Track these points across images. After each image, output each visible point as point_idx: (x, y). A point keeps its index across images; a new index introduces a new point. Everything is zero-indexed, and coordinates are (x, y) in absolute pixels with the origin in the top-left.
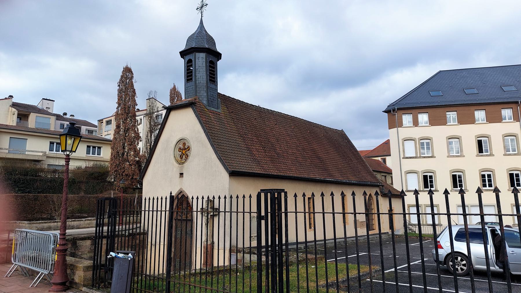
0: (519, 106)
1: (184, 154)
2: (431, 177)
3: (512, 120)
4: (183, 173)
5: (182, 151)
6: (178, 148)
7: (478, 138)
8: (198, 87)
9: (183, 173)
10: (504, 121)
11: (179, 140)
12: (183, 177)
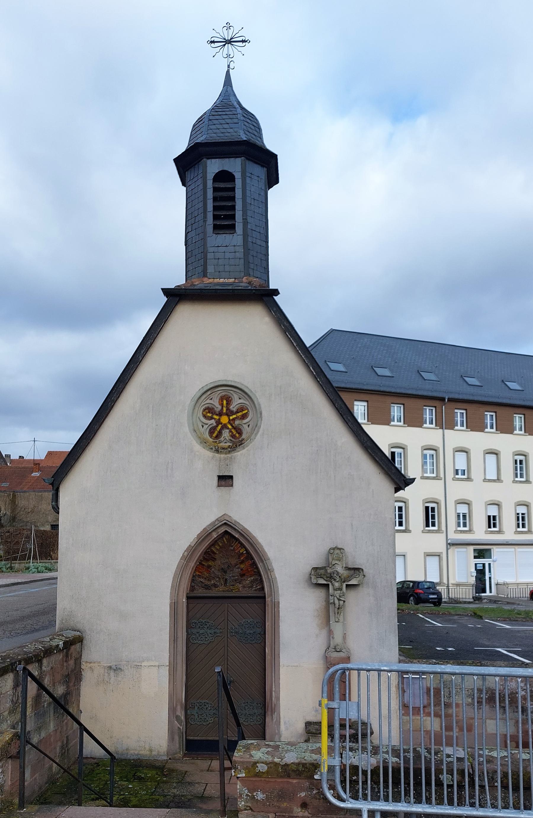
0: (445, 404)
1: (225, 426)
2: (433, 509)
3: (402, 423)
4: (231, 477)
5: (217, 417)
6: (204, 407)
7: (392, 448)
8: (251, 253)
9: (231, 477)
10: (392, 423)
11: (233, 384)
12: (232, 486)
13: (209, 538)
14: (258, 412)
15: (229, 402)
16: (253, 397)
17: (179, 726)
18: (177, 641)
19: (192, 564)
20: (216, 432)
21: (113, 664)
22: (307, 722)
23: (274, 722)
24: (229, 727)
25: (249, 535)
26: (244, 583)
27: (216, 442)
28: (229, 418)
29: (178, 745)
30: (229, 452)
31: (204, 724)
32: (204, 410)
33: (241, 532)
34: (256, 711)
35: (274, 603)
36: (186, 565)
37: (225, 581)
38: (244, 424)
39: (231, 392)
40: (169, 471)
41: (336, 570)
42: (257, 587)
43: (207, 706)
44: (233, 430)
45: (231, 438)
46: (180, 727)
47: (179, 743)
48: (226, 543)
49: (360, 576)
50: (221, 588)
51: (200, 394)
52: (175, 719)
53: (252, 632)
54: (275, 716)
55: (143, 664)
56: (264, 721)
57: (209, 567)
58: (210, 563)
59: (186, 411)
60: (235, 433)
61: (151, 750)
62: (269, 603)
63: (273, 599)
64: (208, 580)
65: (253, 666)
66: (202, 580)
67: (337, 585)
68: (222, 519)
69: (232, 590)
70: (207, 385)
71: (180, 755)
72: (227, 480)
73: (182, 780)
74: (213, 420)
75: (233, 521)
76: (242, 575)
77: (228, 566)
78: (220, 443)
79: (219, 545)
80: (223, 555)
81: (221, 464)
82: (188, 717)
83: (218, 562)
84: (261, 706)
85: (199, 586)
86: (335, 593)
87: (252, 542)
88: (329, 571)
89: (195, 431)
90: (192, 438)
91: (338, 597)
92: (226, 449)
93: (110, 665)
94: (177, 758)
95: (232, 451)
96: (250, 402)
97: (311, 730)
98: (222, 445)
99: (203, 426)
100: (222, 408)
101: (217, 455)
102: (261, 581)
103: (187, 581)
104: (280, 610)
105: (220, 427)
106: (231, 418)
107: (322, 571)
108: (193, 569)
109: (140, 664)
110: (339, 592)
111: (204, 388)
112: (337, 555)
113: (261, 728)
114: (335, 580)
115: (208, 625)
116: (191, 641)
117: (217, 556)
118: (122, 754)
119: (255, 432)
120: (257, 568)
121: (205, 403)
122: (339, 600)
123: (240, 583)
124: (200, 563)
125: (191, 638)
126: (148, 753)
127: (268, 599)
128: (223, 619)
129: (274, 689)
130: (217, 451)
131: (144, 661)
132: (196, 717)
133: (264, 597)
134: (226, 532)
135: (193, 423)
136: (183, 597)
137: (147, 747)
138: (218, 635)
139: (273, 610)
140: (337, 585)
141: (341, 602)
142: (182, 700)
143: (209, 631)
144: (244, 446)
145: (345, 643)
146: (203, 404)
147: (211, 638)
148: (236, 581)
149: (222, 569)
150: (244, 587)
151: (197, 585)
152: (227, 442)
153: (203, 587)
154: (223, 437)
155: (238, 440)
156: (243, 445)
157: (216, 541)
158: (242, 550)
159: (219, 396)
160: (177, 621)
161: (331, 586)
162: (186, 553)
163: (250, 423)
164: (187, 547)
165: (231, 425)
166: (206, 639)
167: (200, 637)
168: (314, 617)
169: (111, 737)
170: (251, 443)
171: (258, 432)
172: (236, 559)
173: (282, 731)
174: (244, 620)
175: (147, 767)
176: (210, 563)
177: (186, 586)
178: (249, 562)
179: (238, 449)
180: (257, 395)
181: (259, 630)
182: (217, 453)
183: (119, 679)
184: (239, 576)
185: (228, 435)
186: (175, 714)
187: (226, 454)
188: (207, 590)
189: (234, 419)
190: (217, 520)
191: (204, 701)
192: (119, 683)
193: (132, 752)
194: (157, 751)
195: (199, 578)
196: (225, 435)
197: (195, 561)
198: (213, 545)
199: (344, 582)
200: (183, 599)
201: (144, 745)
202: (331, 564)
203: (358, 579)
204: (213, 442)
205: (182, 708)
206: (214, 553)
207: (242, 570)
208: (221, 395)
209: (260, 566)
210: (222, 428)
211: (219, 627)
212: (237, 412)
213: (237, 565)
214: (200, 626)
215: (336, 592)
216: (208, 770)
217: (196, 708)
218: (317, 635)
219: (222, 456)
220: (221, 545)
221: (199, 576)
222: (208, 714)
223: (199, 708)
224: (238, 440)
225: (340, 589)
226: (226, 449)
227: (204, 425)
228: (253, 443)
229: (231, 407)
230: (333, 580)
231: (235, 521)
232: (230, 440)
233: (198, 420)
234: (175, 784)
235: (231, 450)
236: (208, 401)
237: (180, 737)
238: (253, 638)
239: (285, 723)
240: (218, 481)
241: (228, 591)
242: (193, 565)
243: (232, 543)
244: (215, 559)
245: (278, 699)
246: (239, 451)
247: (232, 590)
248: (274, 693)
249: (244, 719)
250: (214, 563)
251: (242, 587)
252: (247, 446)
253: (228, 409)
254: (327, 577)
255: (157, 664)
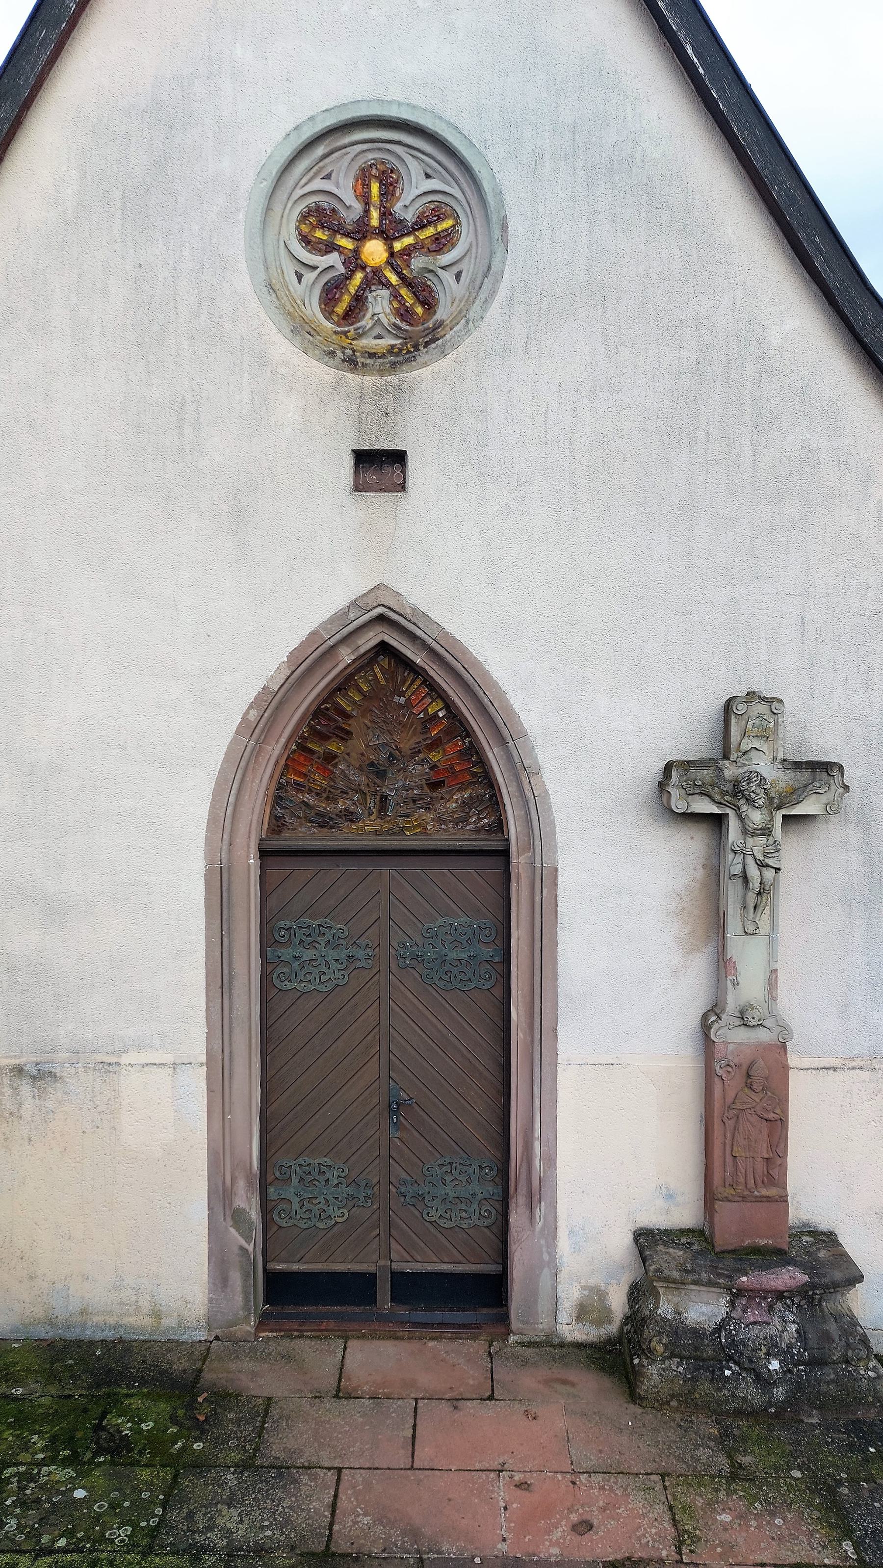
1: (375, 278)
4: (398, 458)
5: (346, 243)
6: (301, 207)
9: (398, 458)
11: (405, 114)
12: (402, 487)
13: (329, 666)
14: (494, 218)
15: (389, 189)
16: (476, 166)
17: (243, 1242)
18: (230, 990)
19: (275, 750)
20: (346, 299)
21: (27, 1060)
22: (641, 1229)
23: (537, 1230)
24: (393, 1232)
25: (459, 656)
26: (440, 807)
27: (345, 333)
28: (390, 247)
29: (239, 1299)
30: (394, 365)
31: (321, 1225)
32: (304, 217)
33: (434, 645)
34: (478, 1190)
35: (538, 872)
36: (257, 752)
37: (381, 801)
38: (442, 268)
39: (398, 149)
40: (188, 431)
41: (753, 768)
42: (480, 819)
43: (328, 1175)
44: (404, 292)
45: (398, 322)
46: (246, 1245)
47: (246, 1293)
48: (383, 682)
49: (833, 787)
50: (370, 824)
51: (287, 151)
52: (230, 1222)
53: (464, 956)
54: (540, 1213)
55: (125, 1059)
56: (500, 1218)
57: (330, 758)
58: (333, 747)
59: (241, 216)
60: (410, 300)
61: (157, 1315)
62: (521, 871)
63: (538, 858)
64: (328, 798)
65: (469, 1056)
66: (308, 798)
67: (757, 817)
68: (371, 601)
69: (402, 830)
70: (312, 119)
71: (249, 1327)
72: (387, 469)
73: (256, 1450)
74: (335, 255)
75: (409, 611)
76: (435, 785)
77: (391, 755)
78: (359, 336)
79: (360, 690)
80: (372, 721)
81: (366, 408)
82: (269, 1208)
83: (358, 744)
84: (494, 1173)
85: (299, 817)
86: (749, 845)
87: (471, 681)
88: (727, 773)
89: (271, 287)
90: (263, 315)
91: (759, 856)
92: (383, 356)
93: (17, 1062)
94: (239, 1335)
95: (401, 363)
96: (465, 185)
97: (666, 1272)
98: (368, 342)
99: (299, 277)
100: (367, 212)
101: (349, 375)
102: (495, 803)
103: (259, 802)
104: (560, 892)
105: (359, 276)
106: (398, 246)
107: (707, 774)
108: (277, 762)
109: (117, 1060)
110: (762, 840)
111: (305, 128)
112: (757, 722)
113: (493, 1237)
114: (750, 801)
115: (328, 936)
116: (276, 982)
117: (353, 726)
118: (69, 1327)
119: (482, 296)
120: (482, 762)
121: (308, 189)
122: (762, 865)
123: (428, 809)
124: (298, 745)
125: (275, 976)
126: (147, 1321)
127: (518, 861)
128: (375, 917)
129: (537, 1134)
130: (352, 363)
131: (126, 1051)
132: (296, 1206)
133: (505, 854)
134: (383, 648)
135: (265, 261)
136: (248, 852)
137: (145, 1304)
138: (359, 964)
139: (538, 891)
140: (757, 817)
141: (769, 874)
142: (251, 1163)
143: (332, 954)
144: (443, 345)
145: (774, 999)
146: (299, 192)
147: (338, 975)
148: (414, 801)
149: (372, 764)
150: (440, 821)
151: (293, 815)
152: (383, 333)
153: (310, 821)
154: (369, 315)
155: (421, 328)
156: (440, 342)
157: (351, 676)
158: (436, 708)
159: (357, 165)
160: (229, 928)
161: (733, 824)
162: (253, 715)
163: (463, 266)
164: (255, 694)
165: (399, 274)
166: (324, 979)
167: (304, 972)
168: (668, 914)
169: (31, 1278)
170: (468, 333)
171: (493, 293)
172: (414, 734)
173: (561, 1257)
174: (441, 921)
175: (143, 1382)
176: (333, 747)
177: (255, 818)
178: (457, 745)
179: (423, 355)
180: (490, 157)
181: (486, 952)
182: (351, 371)
183: (50, 1104)
184: (426, 788)
185: (388, 311)
186: (231, 1204)
187: (381, 372)
188: (325, 830)
189: (407, 252)
190: (354, 604)
191: (317, 1161)
192: (50, 1116)
193: (97, 1319)
194: (175, 1314)
195: (298, 791)
196: (378, 309)
197: (283, 740)
198: (339, 689)
199: (779, 808)
200: (248, 858)
201: (134, 1298)
202: (738, 749)
203: (824, 799)
204: (336, 333)
205: (250, 1184)
206: (346, 716)
207: (433, 767)
208: (360, 162)
209: (494, 756)
210: (366, 284)
211: (363, 941)
212: (419, 225)
213: (419, 752)
214: (304, 938)
215: (750, 841)
216: (338, 1389)
217: (295, 1180)
218: (675, 972)
219: (370, 380)
220: (365, 689)
221: (299, 787)
222: (330, 1198)
223: (302, 1179)
224: (421, 328)
225: (766, 831)
226: (383, 356)
227: (303, 271)
228: (476, 334)
229: (397, 208)
230: (743, 801)
231: (415, 610)
232: (395, 325)
233: (283, 251)
234: (231, 1478)
235: (400, 359)
236: (318, 184)
237: (246, 1276)
238: (470, 974)
239: (571, 1232)
240: (356, 472)
241: (390, 832)
242: (277, 752)
243: (404, 682)
244: (349, 733)
245: (551, 1161)
246: (426, 365)
247: (402, 830)
248: (537, 1144)
249: (440, 1213)
250: (345, 747)
251: (433, 820)
252: (454, 347)
253: (385, 214)
254: (723, 793)
255: (169, 1058)
